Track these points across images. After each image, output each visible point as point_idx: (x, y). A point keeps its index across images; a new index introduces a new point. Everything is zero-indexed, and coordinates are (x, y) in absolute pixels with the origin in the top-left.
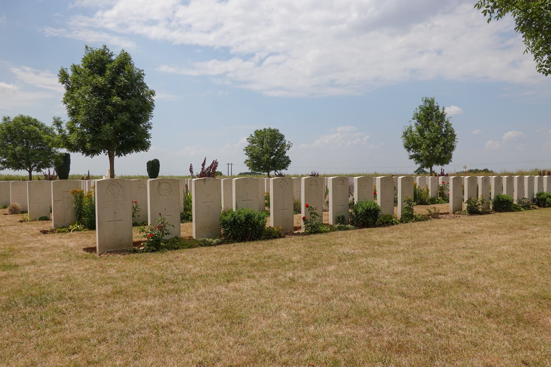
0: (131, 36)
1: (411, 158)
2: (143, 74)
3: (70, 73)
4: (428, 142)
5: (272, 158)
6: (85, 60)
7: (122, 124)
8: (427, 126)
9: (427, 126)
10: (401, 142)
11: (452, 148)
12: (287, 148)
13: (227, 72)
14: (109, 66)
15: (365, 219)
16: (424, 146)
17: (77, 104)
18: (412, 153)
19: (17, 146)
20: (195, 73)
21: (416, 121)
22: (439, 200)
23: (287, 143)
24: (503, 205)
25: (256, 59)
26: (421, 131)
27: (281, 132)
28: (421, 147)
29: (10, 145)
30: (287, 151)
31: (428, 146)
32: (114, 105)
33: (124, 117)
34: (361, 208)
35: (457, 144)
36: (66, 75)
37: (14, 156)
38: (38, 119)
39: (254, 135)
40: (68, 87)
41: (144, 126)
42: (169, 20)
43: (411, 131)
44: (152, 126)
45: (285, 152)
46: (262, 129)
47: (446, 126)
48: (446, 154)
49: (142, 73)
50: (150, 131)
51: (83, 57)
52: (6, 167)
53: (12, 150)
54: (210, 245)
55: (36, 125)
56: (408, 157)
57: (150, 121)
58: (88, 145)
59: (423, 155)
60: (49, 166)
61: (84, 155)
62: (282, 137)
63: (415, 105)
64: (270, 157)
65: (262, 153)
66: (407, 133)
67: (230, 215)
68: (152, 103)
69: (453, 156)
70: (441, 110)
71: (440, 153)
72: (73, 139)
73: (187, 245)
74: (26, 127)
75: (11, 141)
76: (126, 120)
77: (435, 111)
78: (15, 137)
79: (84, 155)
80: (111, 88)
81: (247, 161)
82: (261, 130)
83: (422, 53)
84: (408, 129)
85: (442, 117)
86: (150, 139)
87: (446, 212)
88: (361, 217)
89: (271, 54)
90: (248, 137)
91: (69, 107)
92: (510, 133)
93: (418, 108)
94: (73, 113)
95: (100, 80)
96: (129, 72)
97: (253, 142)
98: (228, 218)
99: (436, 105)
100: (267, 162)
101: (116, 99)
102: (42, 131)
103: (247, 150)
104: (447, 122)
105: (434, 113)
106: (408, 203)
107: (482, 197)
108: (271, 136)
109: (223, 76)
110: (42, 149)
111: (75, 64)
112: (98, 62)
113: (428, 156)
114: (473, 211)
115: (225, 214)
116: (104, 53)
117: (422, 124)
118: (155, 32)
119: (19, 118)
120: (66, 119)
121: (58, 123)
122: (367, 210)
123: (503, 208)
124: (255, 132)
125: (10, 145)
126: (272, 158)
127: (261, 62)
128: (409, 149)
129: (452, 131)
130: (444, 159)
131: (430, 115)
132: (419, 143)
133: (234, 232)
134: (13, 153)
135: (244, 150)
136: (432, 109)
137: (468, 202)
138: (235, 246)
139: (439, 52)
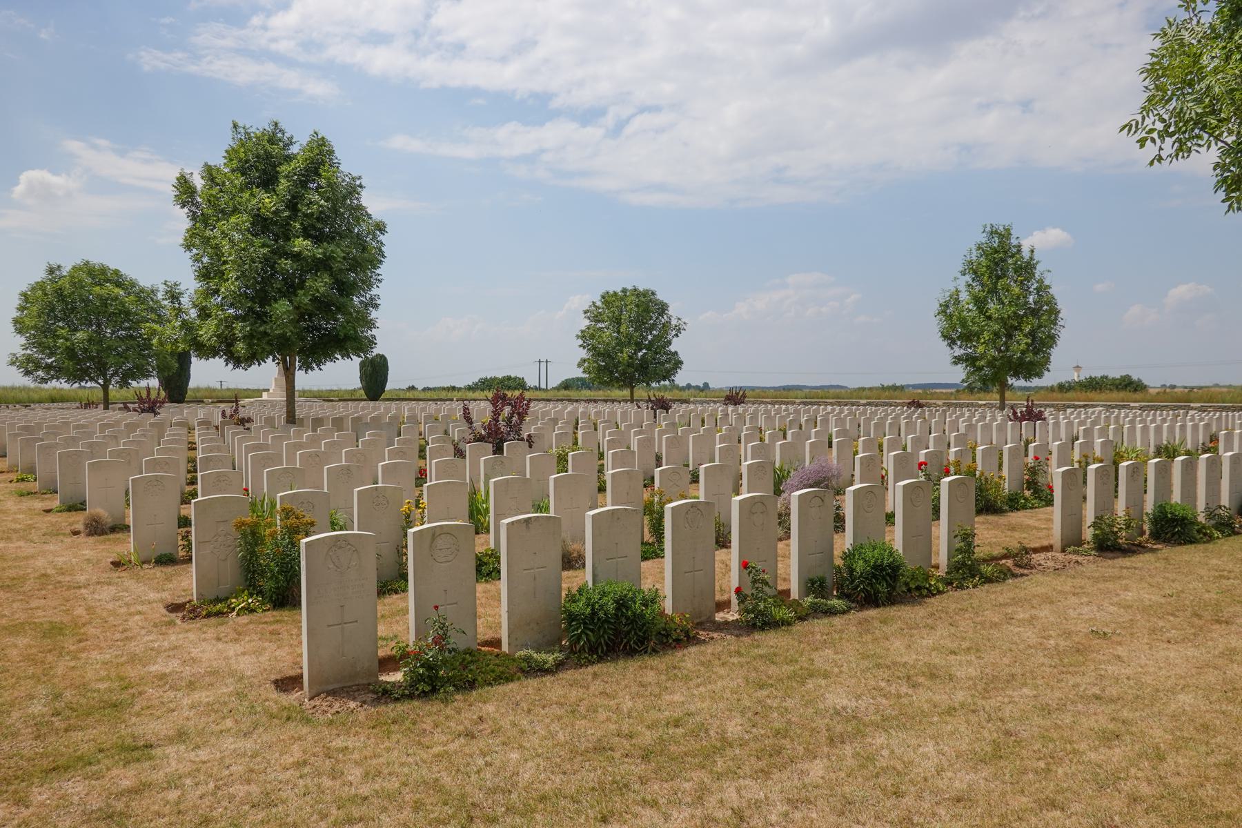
0: (329, 70)
1: (955, 363)
2: (361, 186)
3: (199, 182)
4: (997, 327)
5: (640, 354)
6: (231, 154)
7: (314, 300)
8: (993, 291)
9: (993, 291)
10: (933, 326)
11: (1051, 340)
12: (674, 332)
13: (543, 151)
14: (284, 169)
15: (871, 584)
16: (986, 336)
17: (217, 253)
18: (958, 352)
19: (76, 330)
20: (467, 152)
21: (968, 278)
22: (1026, 499)
23: (674, 322)
24: (1173, 528)
25: (610, 120)
26: (980, 303)
27: (660, 296)
28: (979, 338)
29: (62, 328)
30: (675, 340)
31: (997, 335)
32: (297, 257)
33: (321, 284)
34: (861, 562)
35: (1063, 330)
36: (190, 187)
37: (71, 353)
38: (123, 271)
39: (599, 304)
40: (194, 213)
41: (361, 302)
42: (417, 34)
43: (957, 301)
44: (378, 302)
45: (670, 343)
46: (619, 290)
47: (1038, 290)
48: (1036, 353)
49: (358, 182)
50: (374, 314)
51: (227, 147)
52: (52, 378)
53: (67, 340)
54: (541, 670)
55: (118, 285)
56: (949, 359)
57: (374, 291)
58: (240, 347)
59: (983, 356)
60: (146, 375)
61: (231, 366)
62: (662, 308)
63: (968, 241)
64: (635, 353)
65: (617, 344)
66: (947, 307)
67: (583, 600)
68: (380, 250)
69: (1052, 358)
70: (1026, 254)
71: (1023, 352)
72: (207, 332)
73: (493, 671)
74: (97, 289)
75: (62, 319)
76: (322, 290)
77: (1012, 256)
78: (73, 309)
79: (231, 366)
80: (289, 217)
81: (584, 361)
82: (615, 293)
83: (986, 107)
84: (951, 296)
85: (1026, 269)
86: (374, 332)
87: (1045, 543)
88: (862, 582)
89: (643, 109)
90: (586, 308)
91: (197, 259)
92: (1182, 289)
93: (974, 248)
94: (205, 275)
95: (267, 202)
96: (330, 185)
97: (597, 318)
98: (580, 607)
99: (1014, 242)
100: (629, 365)
101: (300, 244)
102: (132, 298)
103: (583, 337)
104: (1041, 281)
105: (1010, 261)
106: (964, 540)
107: (1128, 514)
108: (637, 306)
109: (530, 159)
110: (131, 336)
111: (211, 163)
112: (261, 161)
113: (994, 359)
114: (1107, 546)
115: (572, 599)
116: (272, 140)
117: (982, 285)
118: (382, 61)
119: (81, 269)
120: (190, 285)
121: (174, 296)
122: (875, 567)
123: (1173, 535)
124: (603, 297)
125: (62, 328)
126: (640, 354)
127: (619, 128)
128: (952, 343)
129: (1051, 302)
130: (1031, 367)
131: (1001, 264)
132: (975, 328)
133: (593, 639)
134: (67, 348)
135: (578, 336)
136: (1006, 252)
137: (1094, 525)
138: (595, 675)
139: (1026, 105)
